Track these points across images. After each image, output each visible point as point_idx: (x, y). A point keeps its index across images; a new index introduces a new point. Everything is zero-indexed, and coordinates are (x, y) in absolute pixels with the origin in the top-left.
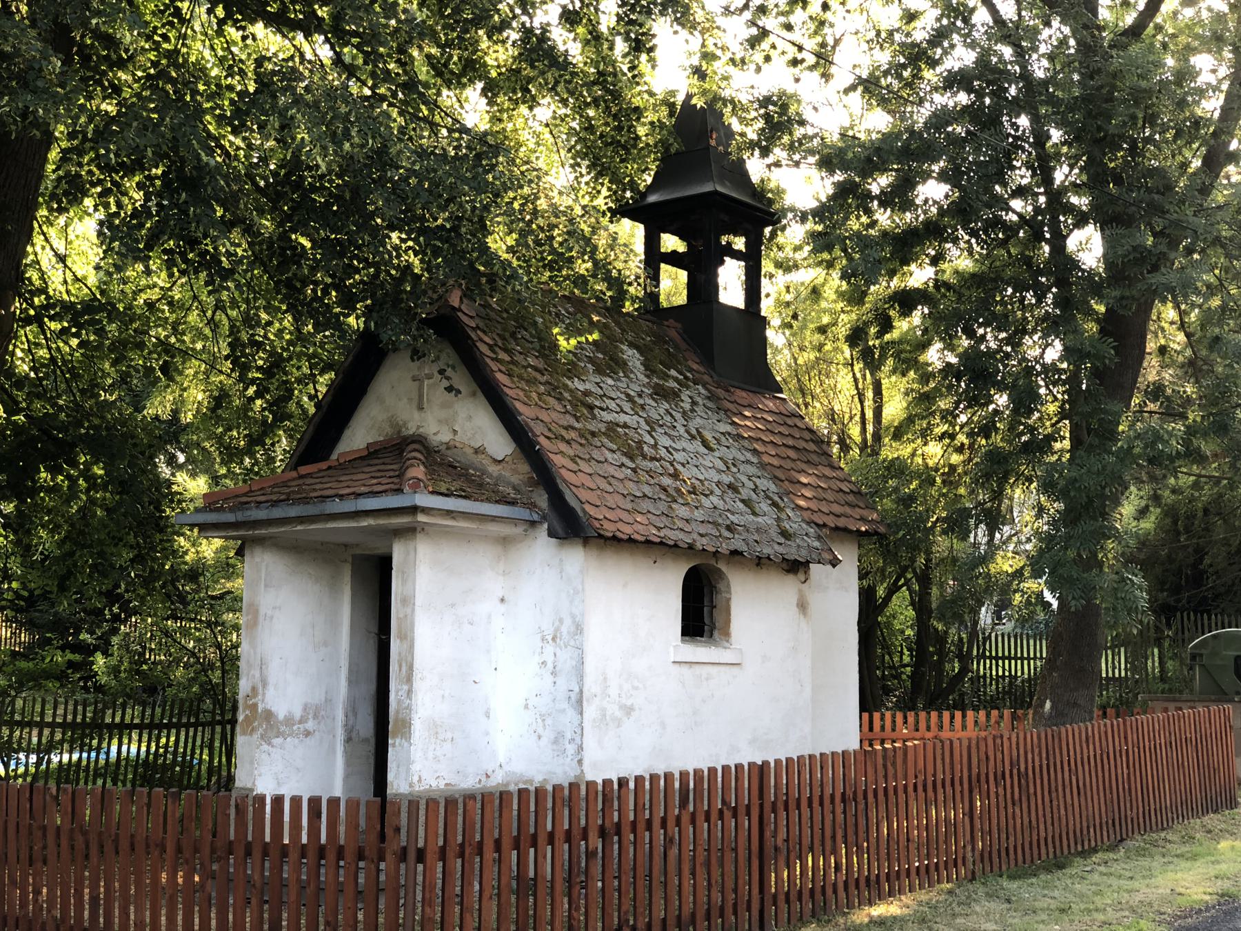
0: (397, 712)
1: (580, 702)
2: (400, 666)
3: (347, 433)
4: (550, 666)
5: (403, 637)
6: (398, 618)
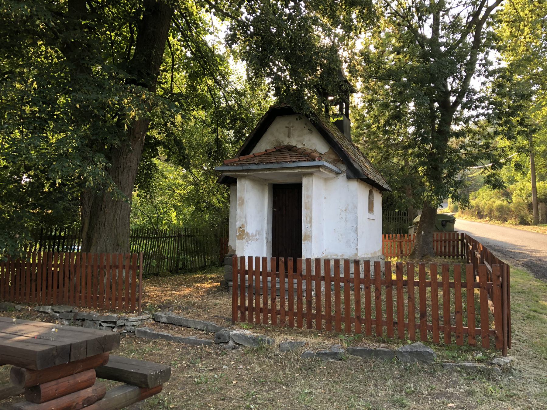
0: (306, 233)
1: (356, 230)
3: (258, 145)
4: (344, 219)
5: (307, 208)
6: (305, 202)
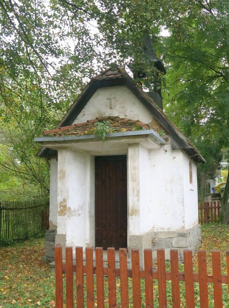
0: (133, 207)
1: (183, 202)
2: (134, 191)
5: (134, 180)
6: (132, 174)
